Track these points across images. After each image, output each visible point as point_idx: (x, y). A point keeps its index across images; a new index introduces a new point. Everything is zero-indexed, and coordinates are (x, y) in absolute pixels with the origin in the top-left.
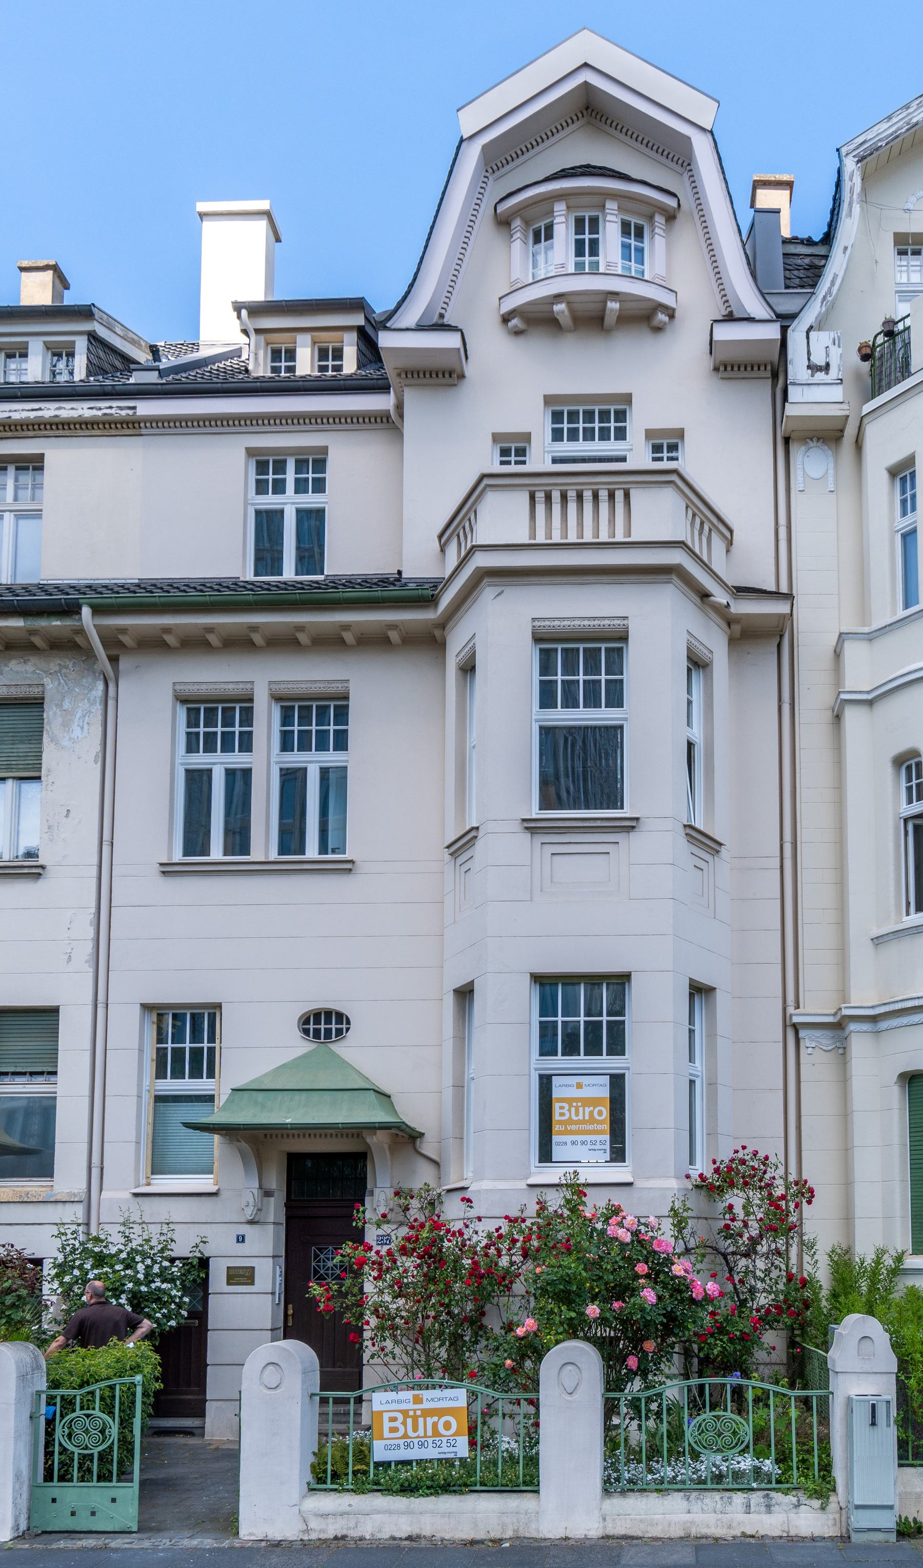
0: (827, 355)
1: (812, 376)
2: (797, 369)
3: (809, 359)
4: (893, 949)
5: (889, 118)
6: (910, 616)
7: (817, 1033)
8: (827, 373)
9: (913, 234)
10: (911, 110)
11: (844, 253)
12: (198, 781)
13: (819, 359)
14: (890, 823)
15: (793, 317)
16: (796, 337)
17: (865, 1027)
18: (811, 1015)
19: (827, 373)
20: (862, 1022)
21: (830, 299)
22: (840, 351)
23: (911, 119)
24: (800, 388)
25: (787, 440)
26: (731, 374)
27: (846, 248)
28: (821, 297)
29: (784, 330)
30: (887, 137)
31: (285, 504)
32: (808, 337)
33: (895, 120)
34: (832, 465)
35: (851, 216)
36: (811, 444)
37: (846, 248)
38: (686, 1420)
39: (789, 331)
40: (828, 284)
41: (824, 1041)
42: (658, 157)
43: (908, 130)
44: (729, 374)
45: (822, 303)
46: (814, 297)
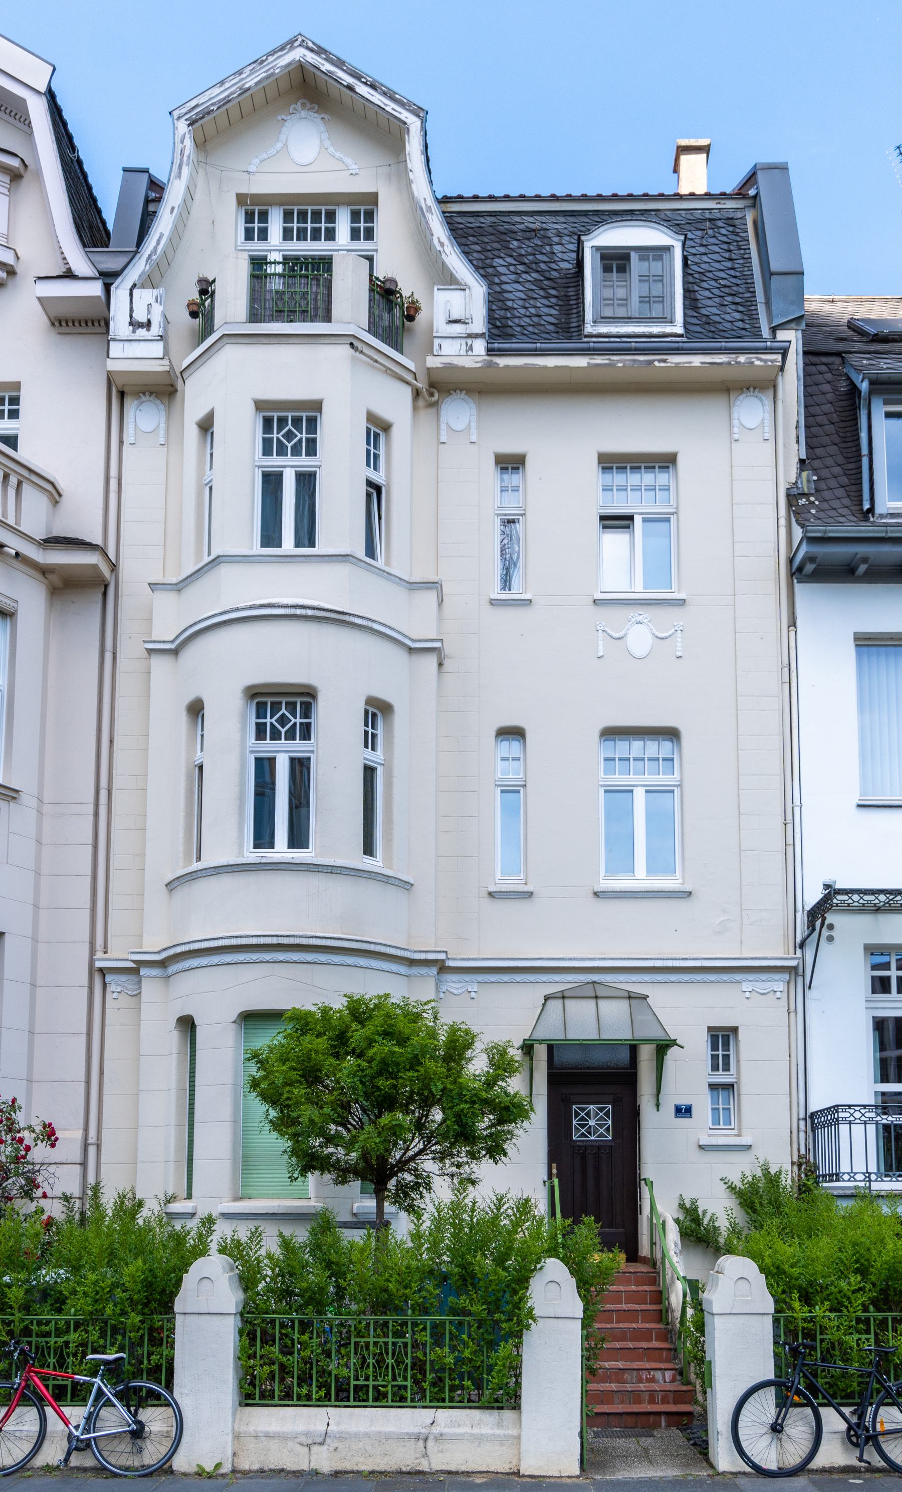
0: (149, 312)
1: (134, 332)
2: (119, 325)
3: (131, 316)
4: (181, 893)
5: (222, 83)
6: (203, 567)
7: (123, 978)
8: (148, 330)
9: (252, 195)
10: (243, 76)
11: (172, 212)
12: (265, 768)
13: (140, 316)
14: (183, 771)
15: (116, 274)
16: (120, 295)
17: (155, 972)
18: (113, 960)
19: (148, 330)
20: (152, 967)
21: (154, 257)
22: (161, 308)
23: (244, 84)
24: (120, 344)
25: (122, 395)
26: (67, 330)
27: (173, 208)
28: (146, 255)
29: (107, 288)
30: (219, 101)
31: (285, 467)
32: (131, 295)
33: (227, 85)
34: (163, 419)
35: (180, 177)
36: (144, 398)
37: (173, 208)
38: (14, 1372)
39: (113, 288)
40: (154, 243)
41: (130, 986)
42: (12, 120)
43: (240, 95)
44: (65, 329)
45: (147, 261)
46: (138, 256)
